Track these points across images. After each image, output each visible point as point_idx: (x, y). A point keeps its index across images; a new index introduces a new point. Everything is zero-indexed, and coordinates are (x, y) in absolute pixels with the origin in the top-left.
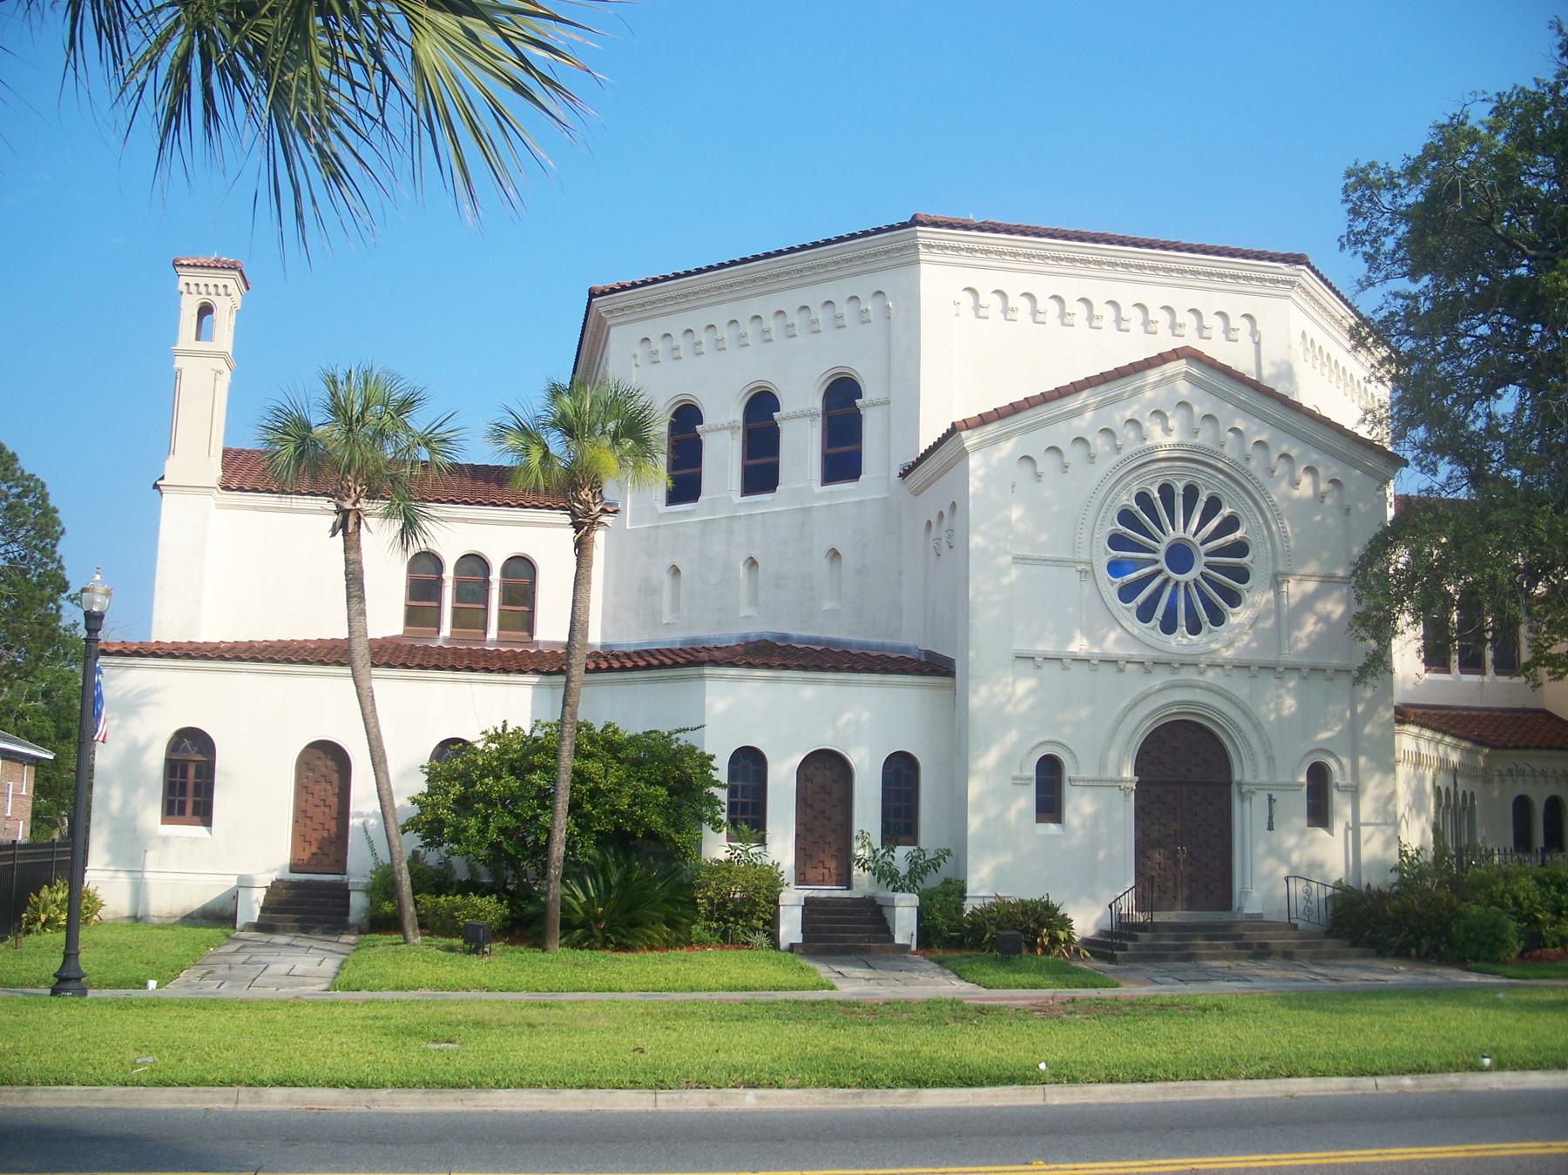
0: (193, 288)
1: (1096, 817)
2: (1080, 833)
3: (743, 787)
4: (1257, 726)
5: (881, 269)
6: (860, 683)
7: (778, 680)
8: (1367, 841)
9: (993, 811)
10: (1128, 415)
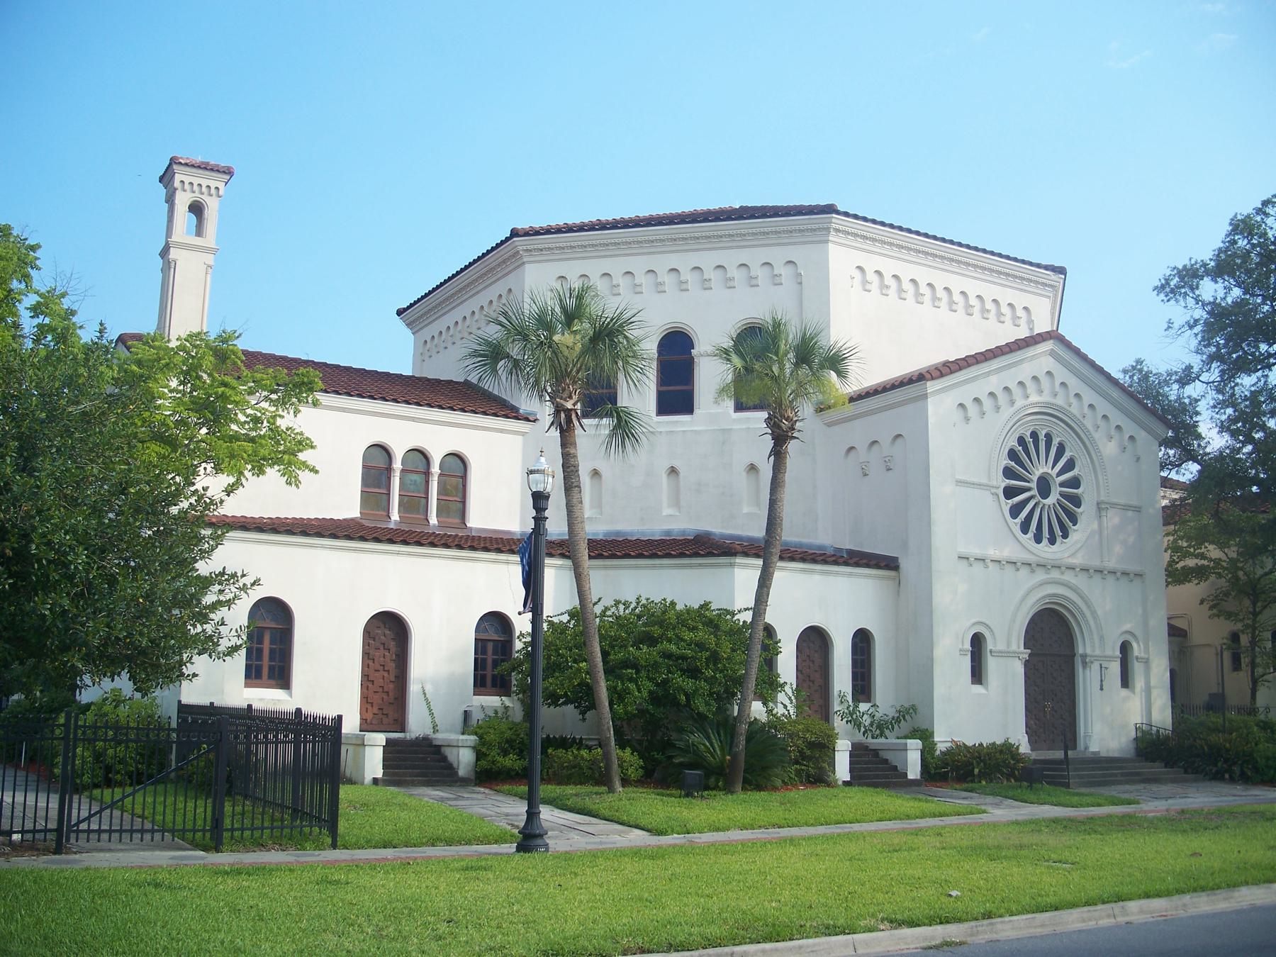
0: (187, 186)
5: (794, 244)
6: (837, 573)
7: (812, 571)
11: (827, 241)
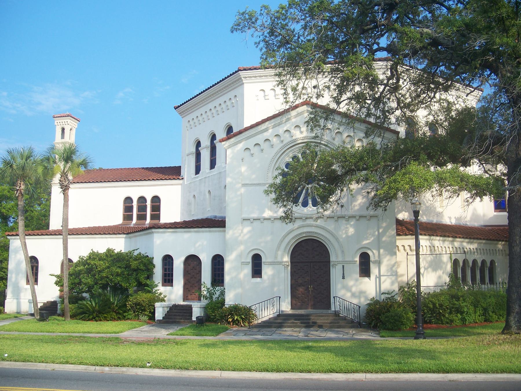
1: (273, 276)
2: (267, 282)
3: (168, 268)
4: (337, 239)
6: (203, 232)
7: (176, 232)
8: (383, 282)
9: (234, 275)
10: (285, 129)
11: (243, 84)
